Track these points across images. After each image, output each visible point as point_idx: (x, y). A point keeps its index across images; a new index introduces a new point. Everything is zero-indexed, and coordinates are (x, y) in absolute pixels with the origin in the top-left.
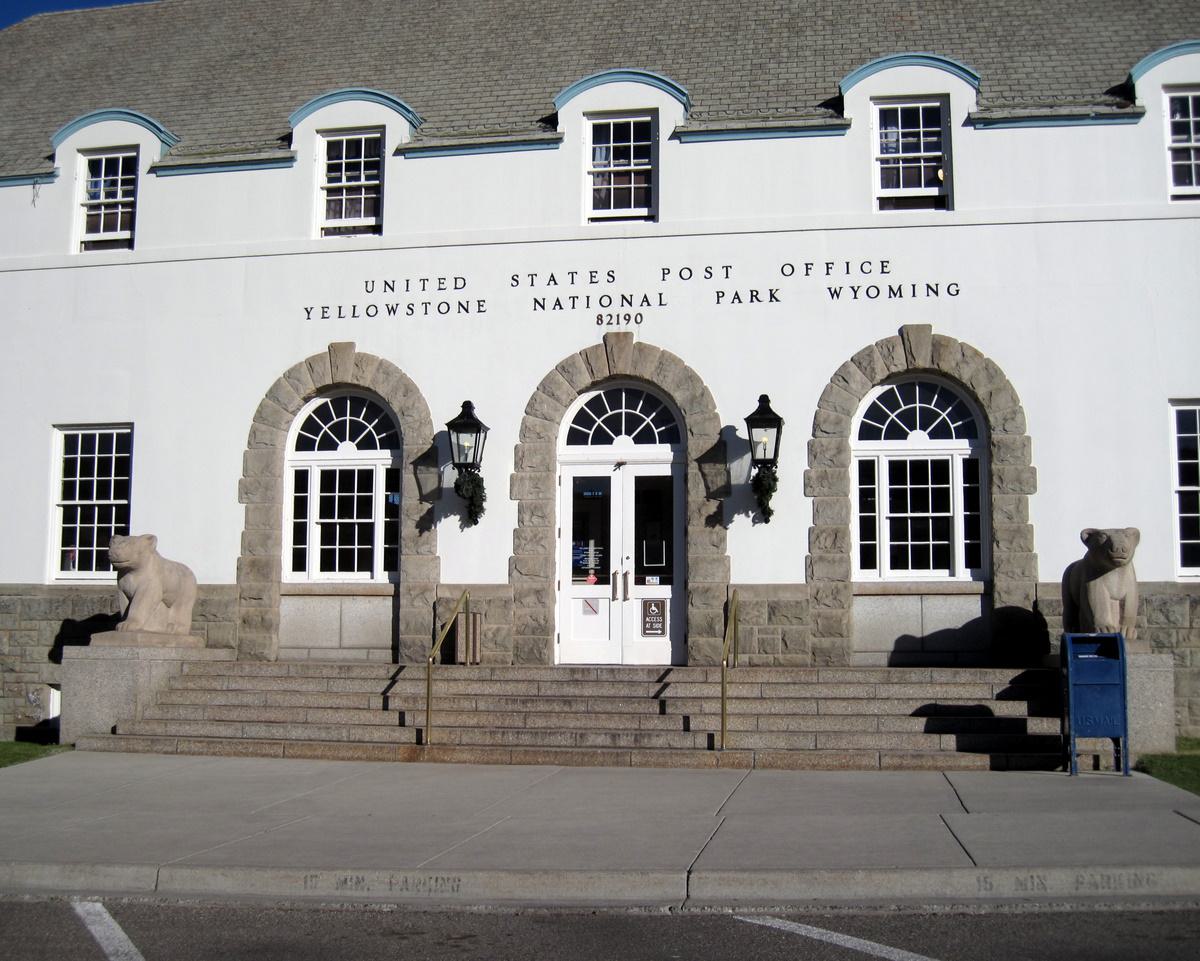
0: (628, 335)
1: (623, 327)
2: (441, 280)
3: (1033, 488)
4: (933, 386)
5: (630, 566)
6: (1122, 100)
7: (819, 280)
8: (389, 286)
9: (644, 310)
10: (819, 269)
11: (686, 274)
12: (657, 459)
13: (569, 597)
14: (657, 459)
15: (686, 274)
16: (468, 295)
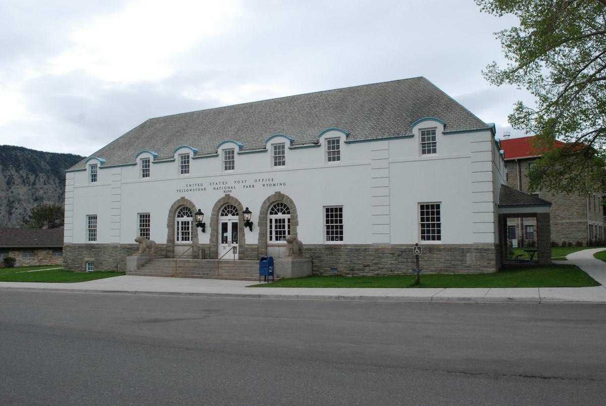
0: (229, 195)
1: (228, 193)
2: (263, 180)
3: (298, 225)
4: (280, 204)
5: (231, 240)
6: (317, 144)
7: (261, 183)
8: (190, 185)
9: (232, 190)
10: (261, 180)
11: (239, 182)
12: (235, 219)
13: (221, 246)
14: (235, 219)
15: (239, 182)
16: (203, 187)
